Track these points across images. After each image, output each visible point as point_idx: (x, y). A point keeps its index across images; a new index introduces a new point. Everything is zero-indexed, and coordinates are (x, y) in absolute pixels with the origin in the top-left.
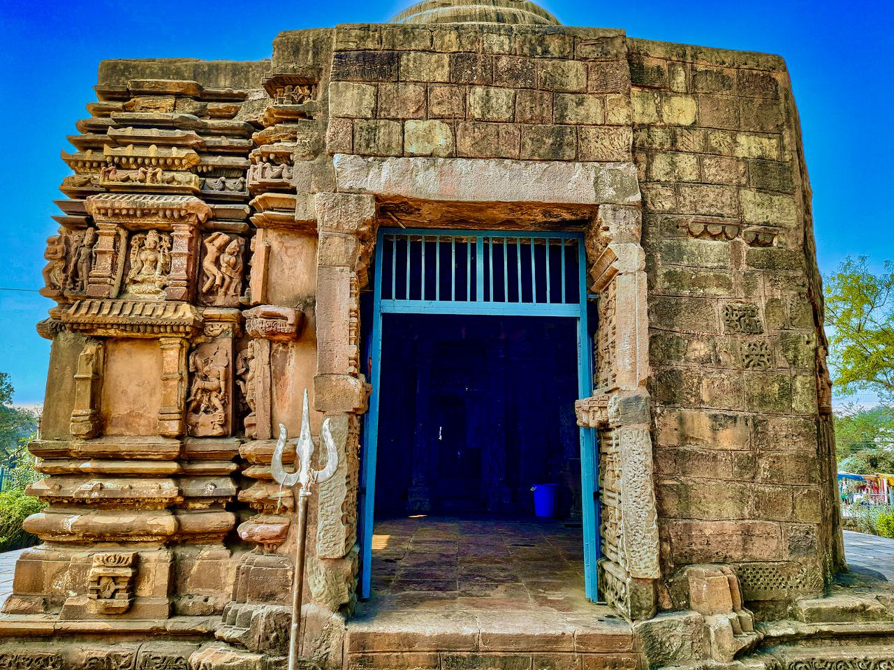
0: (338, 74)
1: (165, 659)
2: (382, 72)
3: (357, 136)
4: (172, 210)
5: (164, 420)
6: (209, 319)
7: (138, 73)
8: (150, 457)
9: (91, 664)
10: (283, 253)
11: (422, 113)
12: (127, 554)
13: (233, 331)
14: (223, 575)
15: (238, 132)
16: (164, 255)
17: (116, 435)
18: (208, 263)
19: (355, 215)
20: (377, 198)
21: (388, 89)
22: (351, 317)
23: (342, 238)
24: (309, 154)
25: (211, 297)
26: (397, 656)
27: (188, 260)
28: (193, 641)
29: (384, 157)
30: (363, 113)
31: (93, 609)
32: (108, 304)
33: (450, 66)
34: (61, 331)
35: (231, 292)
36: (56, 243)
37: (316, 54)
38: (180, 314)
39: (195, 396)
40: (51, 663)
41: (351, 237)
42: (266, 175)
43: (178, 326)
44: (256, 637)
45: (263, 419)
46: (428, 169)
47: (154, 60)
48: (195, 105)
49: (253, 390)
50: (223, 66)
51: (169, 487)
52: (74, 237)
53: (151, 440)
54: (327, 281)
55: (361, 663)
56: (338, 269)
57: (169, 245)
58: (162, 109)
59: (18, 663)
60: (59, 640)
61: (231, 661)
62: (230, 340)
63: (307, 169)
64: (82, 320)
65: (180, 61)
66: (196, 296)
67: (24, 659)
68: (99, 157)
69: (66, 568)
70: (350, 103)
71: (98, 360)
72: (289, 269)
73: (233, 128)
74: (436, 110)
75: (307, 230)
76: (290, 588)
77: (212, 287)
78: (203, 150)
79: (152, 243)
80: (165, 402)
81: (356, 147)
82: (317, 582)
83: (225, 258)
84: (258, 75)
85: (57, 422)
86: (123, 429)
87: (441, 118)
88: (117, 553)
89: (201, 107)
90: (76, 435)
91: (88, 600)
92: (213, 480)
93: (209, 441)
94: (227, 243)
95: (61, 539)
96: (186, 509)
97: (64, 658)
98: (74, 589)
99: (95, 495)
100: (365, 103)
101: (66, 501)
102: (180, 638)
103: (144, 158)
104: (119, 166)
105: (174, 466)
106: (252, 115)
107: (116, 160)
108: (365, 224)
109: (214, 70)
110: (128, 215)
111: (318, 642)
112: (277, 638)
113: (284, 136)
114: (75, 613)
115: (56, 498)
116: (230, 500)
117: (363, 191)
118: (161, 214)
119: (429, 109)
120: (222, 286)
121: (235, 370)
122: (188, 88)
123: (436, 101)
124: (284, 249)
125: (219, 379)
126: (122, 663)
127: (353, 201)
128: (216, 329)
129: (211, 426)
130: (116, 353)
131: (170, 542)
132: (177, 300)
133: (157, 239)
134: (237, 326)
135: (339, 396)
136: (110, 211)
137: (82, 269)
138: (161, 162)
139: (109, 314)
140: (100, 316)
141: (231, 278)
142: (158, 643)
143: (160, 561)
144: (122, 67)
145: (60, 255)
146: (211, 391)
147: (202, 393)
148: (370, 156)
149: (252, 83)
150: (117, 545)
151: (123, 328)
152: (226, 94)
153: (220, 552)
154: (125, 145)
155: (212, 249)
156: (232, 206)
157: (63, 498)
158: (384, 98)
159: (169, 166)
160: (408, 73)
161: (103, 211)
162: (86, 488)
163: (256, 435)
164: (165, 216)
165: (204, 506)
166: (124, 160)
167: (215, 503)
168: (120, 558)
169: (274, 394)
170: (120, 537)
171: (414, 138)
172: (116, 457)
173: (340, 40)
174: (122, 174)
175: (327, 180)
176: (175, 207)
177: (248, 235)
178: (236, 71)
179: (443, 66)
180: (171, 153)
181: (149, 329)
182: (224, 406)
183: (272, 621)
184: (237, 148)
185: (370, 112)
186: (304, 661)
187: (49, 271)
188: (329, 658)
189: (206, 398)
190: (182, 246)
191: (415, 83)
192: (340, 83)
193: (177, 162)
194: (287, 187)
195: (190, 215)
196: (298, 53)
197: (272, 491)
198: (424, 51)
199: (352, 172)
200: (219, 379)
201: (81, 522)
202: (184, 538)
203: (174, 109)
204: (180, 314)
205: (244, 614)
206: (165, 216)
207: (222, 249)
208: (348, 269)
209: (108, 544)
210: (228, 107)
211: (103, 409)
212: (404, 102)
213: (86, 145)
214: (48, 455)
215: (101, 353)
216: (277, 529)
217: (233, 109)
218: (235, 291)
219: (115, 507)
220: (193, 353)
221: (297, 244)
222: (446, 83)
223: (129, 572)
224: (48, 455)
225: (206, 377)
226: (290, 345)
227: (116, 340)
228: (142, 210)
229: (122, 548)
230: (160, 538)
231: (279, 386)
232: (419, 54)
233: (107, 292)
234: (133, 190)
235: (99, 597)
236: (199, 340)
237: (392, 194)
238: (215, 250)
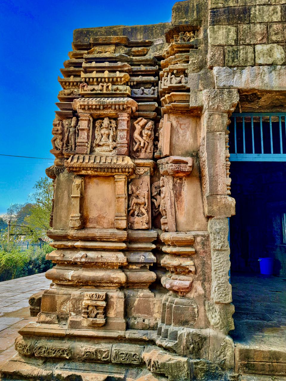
0: (214, 22)
1: (127, 354)
2: (240, 19)
3: (227, 55)
4: (119, 105)
5: (118, 220)
6: (138, 165)
7: (94, 34)
8: (111, 240)
9: (87, 355)
10: (178, 128)
11: (265, 40)
12: (102, 293)
13: (150, 172)
14: (152, 307)
15: (149, 63)
16: (113, 131)
17: (92, 228)
18: (136, 135)
19: (227, 101)
20: (240, 91)
21: (244, 27)
22: (226, 161)
23: (220, 115)
24: (197, 69)
25: (138, 154)
26: (269, 365)
27: (127, 132)
28: (140, 345)
29: (243, 67)
30: (230, 42)
31: (85, 323)
32: (87, 157)
33: (281, 12)
34: (61, 172)
35: (148, 150)
36: (58, 125)
37: (198, 12)
38: (126, 162)
39: (133, 207)
40: (66, 353)
41: (225, 114)
42: (172, 82)
43: (125, 168)
44: (182, 347)
45: (171, 220)
46: (271, 72)
47: (102, 28)
48: (125, 49)
49: (165, 204)
50: (139, 28)
51: (121, 258)
52: (66, 122)
53: (111, 231)
54: (212, 140)
55: (247, 367)
56: (218, 133)
57: (116, 126)
58: (109, 52)
59: (49, 352)
60: (68, 340)
61: (169, 360)
62: (149, 177)
63: (197, 77)
64: (75, 165)
65: (115, 27)
66: (132, 154)
67: (52, 350)
68: (78, 79)
69: (68, 299)
70: (221, 37)
71: (82, 187)
72: (177, 136)
73: (147, 60)
74: (274, 38)
75: (194, 113)
76: (196, 319)
77: (138, 148)
78: (133, 74)
79: (107, 124)
80: (118, 210)
81: (226, 62)
82: (213, 316)
83: (145, 132)
84: (158, 31)
85: (61, 220)
86: (95, 225)
87: (278, 42)
88: (97, 293)
89: (129, 50)
90: (73, 228)
91: (82, 318)
92: (143, 253)
93: (140, 232)
94: (146, 124)
95: (64, 283)
96: (128, 269)
97: (72, 350)
98: (74, 312)
99: (83, 260)
100: (230, 36)
101: (66, 263)
102: (133, 342)
103: (101, 78)
104: (88, 83)
105: (124, 245)
106: (156, 53)
107: (87, 80)
108: (233, 107)
109: (134, 30)
110: (96, 109)
111: (219, 352)
112: (194, 347)
113: (179, 61)
114: (74, 325)
115: (61, 261)
116: (152, 265)
117: (232, 87)
118: (113, 107)
119: (270, 38)
120: (143, 148)
121: (151, 193)
122: (122, 40)
123: (273, 33)
124: (179, 125)
125: (144, 198)
126: (104, 356)
127: (226, 93)
128: (142, 171)
129: (141, 223)
130: (90, 184)
131: (122, 287)
132: (123, 155)
133: (109, 122)
134: (152, 169)
135: (222, 208)
136: (86, 107)
137: (71, 139)
138: (111, 80)
139: (89, 162)
140: (84, 163)
141: (148, 143)
142: (121, 344)
143: (119, 298)
144: (85, 32)
145: (60, 132)
146: (140, 204)
147: (136, 206)
148: (234, 67)
149: (155, 36)
150: (94, 287)
151: (96, 170)
152: (142, 43)
153: (148, 294)
154: (91, 72)
155: (138, 127)
156: (148, 103)
157: (65, 261)
158: (242, 33)
159: (115, 82)
160: (256, 18)
161: (83, 107)
162: (78, 256)
163: (168, 229)
164: (115, 109)
165: (137, 268)
166: (91, 80)
167: (144, 266)
168: (99, 295)
169: (176, 206)
170: (96, 284)
171: (261, 55)
172: (93, 239)
173: (213, 2)
174: (91, 87)
175: (209, 83)
176: (121, 103)
177: (156, 121)
178: (146, 30)
179: (277, 13)
180: (116, 75)
181: (110, 170)
182: (148, 212)
183: (190, 338)
184: (149, 71)
185: (234, 42)
186: (211, 363)
187: (55, 140)
188: (226, 363)
189: (137, 209)
190: (124, 125)
191: (260, 23)
192: (215, 27)
193: (119, 80)
194: (183, 89)
195: (128, 107)
196: (188, 13)
197: (182, 262)
198: (264, 5)
199: (224, 77)
200: (144, 198)
201: (76, 275)
202: (128, 285)
203: (115, 52)
204: (126, 162)
205: (173, 332)
206: (115, 109)
207: (143, 127)
208: (224, 133)
209: (89, 287)
210: (143, 49)
211: (85, 213)
212: (254, 35)
213: (69, 74)
214: (56, 238)
215: (83, 183)
216: (188, 283)
217: (146, 51)
218: (150, 150)
219: (92, 266)
220: (131, 184)
221: (187, 122)
222: (280, 22)
223: (104, 304)
224: (56, 238)
225: (138, 196)
226: (184, 179)
227: (90, 177)
228: (103, 106)
229: (97, 290)
230: (117, 285)
231: (178, 202)
232: (262, 7)
233: (86, 151)
234: (97, 95)
235: (88, 317)
236: (133, 177)
237: (249, 88)
238: (140, 128)
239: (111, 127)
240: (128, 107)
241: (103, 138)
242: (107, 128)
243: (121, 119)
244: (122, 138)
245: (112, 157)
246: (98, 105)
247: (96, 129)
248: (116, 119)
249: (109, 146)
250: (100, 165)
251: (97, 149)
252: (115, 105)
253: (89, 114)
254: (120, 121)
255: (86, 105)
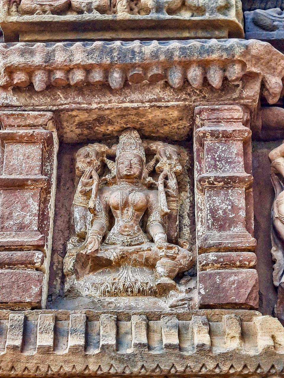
4: (205, 65)
16: (168, 195)
32: (44, 320)
79: (135, 160)
110: (85, 88)
118: (176, 79)
133: (142, 153)
140: (30, 352)
161: (20, 77)
195: (248, 77)
239: (154, 173)
240: (248, 77)
241: (116, 229)
242: (133, 180)
243: (212, 134)
244: (221, 222)
245: (179, 317)
246: (100, 65)
247: (79, 188)
248: (185, 141)
249: (153, 266)
250: (121, 360)
251: (89, 285)
252: (186, 66)
253: (49, 114)
254: (208, 142)
255: (39, 68)
